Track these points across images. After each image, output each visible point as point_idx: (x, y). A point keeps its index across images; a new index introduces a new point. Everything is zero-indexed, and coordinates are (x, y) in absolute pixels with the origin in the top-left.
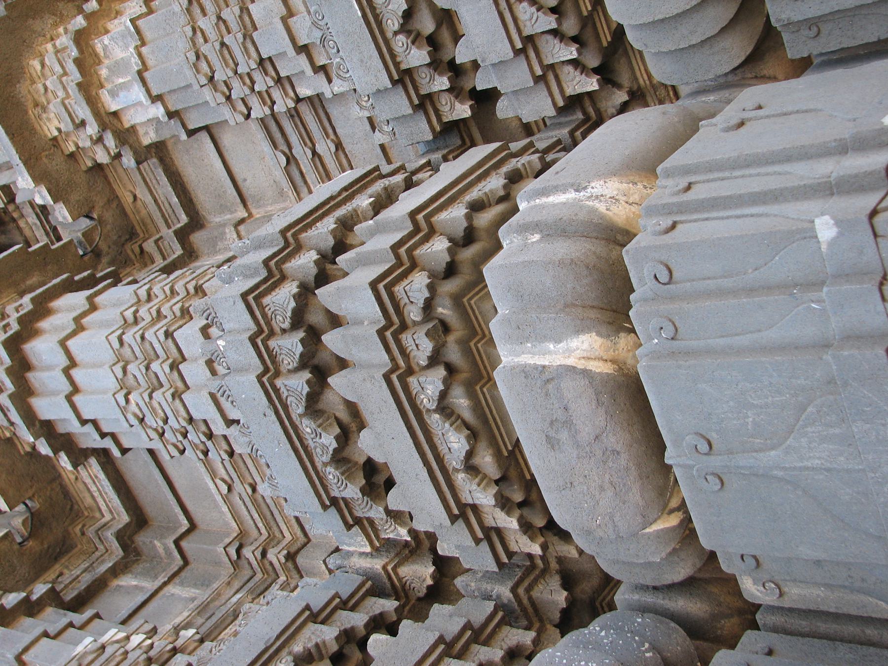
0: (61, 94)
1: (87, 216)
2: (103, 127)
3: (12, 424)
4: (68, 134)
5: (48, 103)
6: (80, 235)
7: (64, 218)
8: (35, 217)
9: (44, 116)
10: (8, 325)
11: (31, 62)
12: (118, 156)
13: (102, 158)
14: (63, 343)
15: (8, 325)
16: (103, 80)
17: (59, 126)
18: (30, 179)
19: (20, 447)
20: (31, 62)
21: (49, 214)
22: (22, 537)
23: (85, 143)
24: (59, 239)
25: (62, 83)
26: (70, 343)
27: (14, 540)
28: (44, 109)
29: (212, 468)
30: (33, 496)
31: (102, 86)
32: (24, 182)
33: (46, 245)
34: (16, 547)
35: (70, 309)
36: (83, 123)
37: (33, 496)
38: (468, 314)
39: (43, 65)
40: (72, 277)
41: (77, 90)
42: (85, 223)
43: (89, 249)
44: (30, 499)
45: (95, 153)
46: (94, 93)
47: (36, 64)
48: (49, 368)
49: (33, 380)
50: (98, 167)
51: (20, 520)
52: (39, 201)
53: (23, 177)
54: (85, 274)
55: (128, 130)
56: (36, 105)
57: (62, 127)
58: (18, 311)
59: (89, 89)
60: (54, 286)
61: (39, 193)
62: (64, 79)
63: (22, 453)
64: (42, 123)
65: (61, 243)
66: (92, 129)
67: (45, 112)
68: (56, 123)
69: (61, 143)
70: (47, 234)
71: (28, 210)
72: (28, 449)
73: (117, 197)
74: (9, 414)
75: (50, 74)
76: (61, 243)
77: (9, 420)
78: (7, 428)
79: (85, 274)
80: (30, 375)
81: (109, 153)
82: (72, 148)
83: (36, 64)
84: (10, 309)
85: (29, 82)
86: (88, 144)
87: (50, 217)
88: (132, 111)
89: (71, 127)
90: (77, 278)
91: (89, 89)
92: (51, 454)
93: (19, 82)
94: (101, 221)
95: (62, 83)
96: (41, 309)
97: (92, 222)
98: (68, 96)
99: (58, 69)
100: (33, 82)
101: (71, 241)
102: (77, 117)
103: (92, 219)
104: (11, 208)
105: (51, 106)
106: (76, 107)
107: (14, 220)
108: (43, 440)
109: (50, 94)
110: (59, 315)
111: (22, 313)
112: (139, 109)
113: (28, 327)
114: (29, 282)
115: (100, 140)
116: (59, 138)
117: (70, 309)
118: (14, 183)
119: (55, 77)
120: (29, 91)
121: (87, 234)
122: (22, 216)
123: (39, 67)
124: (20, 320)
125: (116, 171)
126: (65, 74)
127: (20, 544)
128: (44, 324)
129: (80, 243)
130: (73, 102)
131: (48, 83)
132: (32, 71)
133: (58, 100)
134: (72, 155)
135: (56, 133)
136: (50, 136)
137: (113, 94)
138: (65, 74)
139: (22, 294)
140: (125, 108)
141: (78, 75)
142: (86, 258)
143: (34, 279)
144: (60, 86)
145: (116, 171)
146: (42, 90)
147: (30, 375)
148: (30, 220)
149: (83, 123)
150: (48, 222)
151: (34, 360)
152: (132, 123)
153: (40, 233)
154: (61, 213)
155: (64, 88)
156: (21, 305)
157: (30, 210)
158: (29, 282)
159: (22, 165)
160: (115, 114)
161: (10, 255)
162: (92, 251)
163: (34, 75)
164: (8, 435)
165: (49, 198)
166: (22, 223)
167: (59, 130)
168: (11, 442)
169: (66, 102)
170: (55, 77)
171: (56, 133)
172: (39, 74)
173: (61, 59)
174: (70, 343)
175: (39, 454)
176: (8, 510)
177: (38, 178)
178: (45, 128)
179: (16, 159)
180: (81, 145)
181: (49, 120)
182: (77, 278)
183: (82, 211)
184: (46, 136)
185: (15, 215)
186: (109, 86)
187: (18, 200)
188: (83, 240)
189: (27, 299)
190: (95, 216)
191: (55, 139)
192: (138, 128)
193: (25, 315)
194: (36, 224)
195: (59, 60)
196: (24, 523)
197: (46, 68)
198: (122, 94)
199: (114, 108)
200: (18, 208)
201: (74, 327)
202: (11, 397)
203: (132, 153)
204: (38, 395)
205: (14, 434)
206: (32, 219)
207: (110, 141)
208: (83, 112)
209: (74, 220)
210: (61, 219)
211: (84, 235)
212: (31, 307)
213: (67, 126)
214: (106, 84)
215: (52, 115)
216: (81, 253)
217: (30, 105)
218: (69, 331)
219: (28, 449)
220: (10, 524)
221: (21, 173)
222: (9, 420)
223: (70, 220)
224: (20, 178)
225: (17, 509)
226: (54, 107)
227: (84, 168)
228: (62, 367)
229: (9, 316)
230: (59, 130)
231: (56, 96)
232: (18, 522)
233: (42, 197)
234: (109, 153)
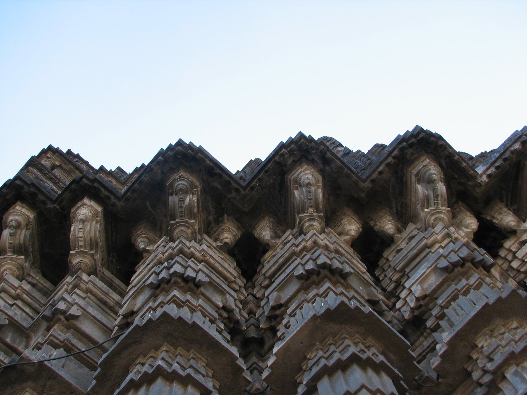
0: (503, 343)
1: (438, 376)
2: (494, 373)
3: (311, 369)
4: (482, 352)
5: (495, 337)
6: (426, 374)
7: (433, 363)
8: (428, 345)
9: (487, 337)
10: (365, 352)
11: (515, 322)
12: (481, 385)
13: (476, 375)
14: (363, 386)
15: (365, 352)
16: (521, 365)
17: (484, 346)
18: (448, 339)
19: (298, 376)
20: (515, 322)
21: (432, 352)
22: (249, 390)
23: (481, 363)
24: (419, 362)
25: (510, 342)
26: (364, 390)
27: (247, 386)
28: (491, 336)
29: (144, 305)
30: (273, 390)
31: (517, 365)
32: (446, 336)
33: (414, 359)
34: (244, 389)
35: (383, 384)
36: (491, 360)
37: (273, 390)
38: (217, 273)
39: (516, 328)
40: (400, 379)
41: (509, 352)
42: (434, 375)
43: (420, 382)
44: (271, 388)
45: (476, 371)
46: (511, 362)
47: (515, 325)
48: (347, 381)
49: (337, 375)
50: (469, 375)
51: (258, 387)
52: (438, 347)
53: (448, 335)
54: (406, 386)
55: (498, 387)
56: (492, 331)
57: (485, 349)
58: (372, 355)
59: (513, 359)
60: (394, 371)
61: (443, 346)
62: (513, 342)
63: (296, 377)
64: (482, 337)
65: (416, 364)
66: (490, 366)
67: (489, 337)
68: (485, 344)
69: (475, 350)
70: (419, 355)
71: (430, 340)
72: (298, 380)
73: (455, 390)
74: (315, 366)
75: (512, 333)
76: (416, 364)
77: (312, 367)
78: (307, 366)
79: (406, 386)
80: (340, 372)
81: (479, 379)
82: (475, 357)
83: (515, 325)
84: (373, 350)
85: (503, 323)
86: (481, 366)
87: (430, 354)
88: (510, 387)
89: (487, 353)
90: (402, 382)
91: (513, 359)
92: (274, 353)
93: (501, 318)
94: (438, 384)
95: (510, 342)
96: (378, 368)
97: (436, 379)
98: (504, 347)
99: (517, 337)
100: (504, 326)
101: (420, 371)
102: (494, 355)
103: (438, 379)
104: (428, 331)
105: (494, 339)
106: (499, 354)
107: (422, 334)
108: (306, 389)
109: (501, 337)
110: (378, 379)
111: (373, 357)
112: (513, 391)
113: (366, 364)
114: (391, 355)
115: (485, 372)
116: (477, 348)
117: (383, 384)
118: (443, 331)
119: (512, 337)
120: (498, 325)
121: (428, 379)
122: (426, 338)
123: (514, 326)
124: (369, 359)
125: (470, 385)
126: (516, 342)
127: (246, 390)
128: (370, 372)
129: (422, 376)
130: (501, 351)
131: (507, 334)
132: (510, 324)
133: (499, 342)
134: (470, 358)
135: (480, 346)
136: (477, 343)
137: (516, 373)
138: (516, 342)
139: (383, 353)
140: (510, 382)
141: (518, 350)
142: (414, 382)
143: (393, 357)
144: (507, 341)
145: (470, 385)
146: (502, 332)
147: (340, 372)
148: (425, 343)
149: (491, 360)
150: (427, 353)
151: (348, 372)
152: (503, 389)
153: (419, 350)
154: (435, 362)
155: (507, 344)
156: (377, 356)
157: (430, 342)
158: (391, 355)
159: (455, 333)
160: (504, 378)
161: (403, 340)
162: (419, 384)
163: (508, 325)
164: (304, 368)
165: (442, 352)
166: (421, 339)
167: (482, 347)
168: (300, 370)
169: (500, 347)
170: (512, 337)
171: (480, 346)
172: (510, 328)
173: (523, 338)
174: (364, 390)
175: (297, 387)
176: (263, 378)
177: (450, 343)
178: (480, 339)
179: (457, 329)
180: (478, 361)
181: (486, 340)
182: (402, 382)
183: (440, 371)
184: (476, 341)
185: (425, 334)
186: (519, 369)
187: (434, 334)
188: (424, 377)
189: (381, 358)
190: (440, 380)
191: (476, 346)
192: (501, 393)
193: (372, 360)
194: (424, 347)
195: (522, 336)
196: (258, 389)
197: (515, 331)
198: (517, 378)
199: (508, 376)
200: (430, 334)
201: (374, 390)
202: (325, 366)
203: (484, 393)
204: (329, 379)
205: (305, 371)
206: (426, 344)
207: (487, 379)
208: (498, 359)
209: (434, 369)
210: (431, 361)
211: (427, 377)
212: (378, 362)
213: (486, 351)
214: (520, 367)
215: (489, 341)
216: (416, 378)
217: (491, 327)
218: (370, 388)
219: (298, 380)
220: (255, 381)
221: (450, 333)
222: (312, 367)
223: (433, 367)
224: (447, 334)
225: (264, 383)
226: (494, 341)
227: (465, 366)
228: (349, 390)
229: (369, 350)
230: (482, 347)
231: (501, 340)
232: (257, 385)
233: (441, 348)
234: (479, 379)
